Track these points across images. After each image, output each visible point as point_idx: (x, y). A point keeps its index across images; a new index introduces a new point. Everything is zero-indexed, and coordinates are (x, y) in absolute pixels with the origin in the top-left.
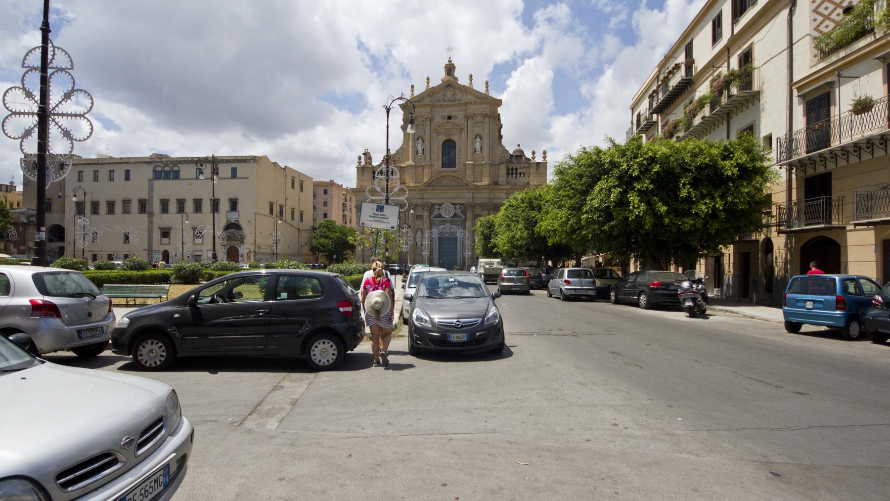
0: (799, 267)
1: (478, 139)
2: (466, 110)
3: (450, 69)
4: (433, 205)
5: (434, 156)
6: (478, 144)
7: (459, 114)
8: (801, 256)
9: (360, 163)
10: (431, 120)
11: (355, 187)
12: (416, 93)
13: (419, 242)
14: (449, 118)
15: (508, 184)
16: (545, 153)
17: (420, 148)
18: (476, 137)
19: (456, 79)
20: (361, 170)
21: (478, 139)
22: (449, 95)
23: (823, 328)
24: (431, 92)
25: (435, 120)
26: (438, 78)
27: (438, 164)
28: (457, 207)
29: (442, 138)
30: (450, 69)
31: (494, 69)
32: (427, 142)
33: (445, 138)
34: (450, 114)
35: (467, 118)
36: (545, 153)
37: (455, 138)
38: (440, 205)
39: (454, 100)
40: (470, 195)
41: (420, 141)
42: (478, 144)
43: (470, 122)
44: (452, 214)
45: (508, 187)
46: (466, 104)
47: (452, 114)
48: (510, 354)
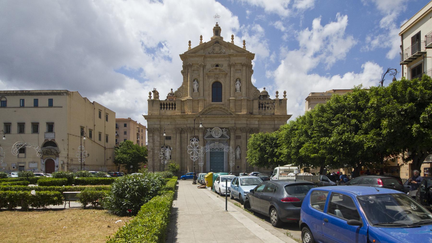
1: (238, 82)
3: (217, 30)
6: (238, 85)
12: (192, 47)
14: (217, 66)
16: (285, 93)
17: (195, 87)
18: (237, 80)
21: (238, 82)
22: (217, 49)
28: (224, 130)
30: (217, 30)
32: (201, 83)
33: (214, 81)
34: (217, 63)
36: (285, 93)
37: (221, 81)
39: (220, 53)
42: (238, 85)
45: (260, 116)
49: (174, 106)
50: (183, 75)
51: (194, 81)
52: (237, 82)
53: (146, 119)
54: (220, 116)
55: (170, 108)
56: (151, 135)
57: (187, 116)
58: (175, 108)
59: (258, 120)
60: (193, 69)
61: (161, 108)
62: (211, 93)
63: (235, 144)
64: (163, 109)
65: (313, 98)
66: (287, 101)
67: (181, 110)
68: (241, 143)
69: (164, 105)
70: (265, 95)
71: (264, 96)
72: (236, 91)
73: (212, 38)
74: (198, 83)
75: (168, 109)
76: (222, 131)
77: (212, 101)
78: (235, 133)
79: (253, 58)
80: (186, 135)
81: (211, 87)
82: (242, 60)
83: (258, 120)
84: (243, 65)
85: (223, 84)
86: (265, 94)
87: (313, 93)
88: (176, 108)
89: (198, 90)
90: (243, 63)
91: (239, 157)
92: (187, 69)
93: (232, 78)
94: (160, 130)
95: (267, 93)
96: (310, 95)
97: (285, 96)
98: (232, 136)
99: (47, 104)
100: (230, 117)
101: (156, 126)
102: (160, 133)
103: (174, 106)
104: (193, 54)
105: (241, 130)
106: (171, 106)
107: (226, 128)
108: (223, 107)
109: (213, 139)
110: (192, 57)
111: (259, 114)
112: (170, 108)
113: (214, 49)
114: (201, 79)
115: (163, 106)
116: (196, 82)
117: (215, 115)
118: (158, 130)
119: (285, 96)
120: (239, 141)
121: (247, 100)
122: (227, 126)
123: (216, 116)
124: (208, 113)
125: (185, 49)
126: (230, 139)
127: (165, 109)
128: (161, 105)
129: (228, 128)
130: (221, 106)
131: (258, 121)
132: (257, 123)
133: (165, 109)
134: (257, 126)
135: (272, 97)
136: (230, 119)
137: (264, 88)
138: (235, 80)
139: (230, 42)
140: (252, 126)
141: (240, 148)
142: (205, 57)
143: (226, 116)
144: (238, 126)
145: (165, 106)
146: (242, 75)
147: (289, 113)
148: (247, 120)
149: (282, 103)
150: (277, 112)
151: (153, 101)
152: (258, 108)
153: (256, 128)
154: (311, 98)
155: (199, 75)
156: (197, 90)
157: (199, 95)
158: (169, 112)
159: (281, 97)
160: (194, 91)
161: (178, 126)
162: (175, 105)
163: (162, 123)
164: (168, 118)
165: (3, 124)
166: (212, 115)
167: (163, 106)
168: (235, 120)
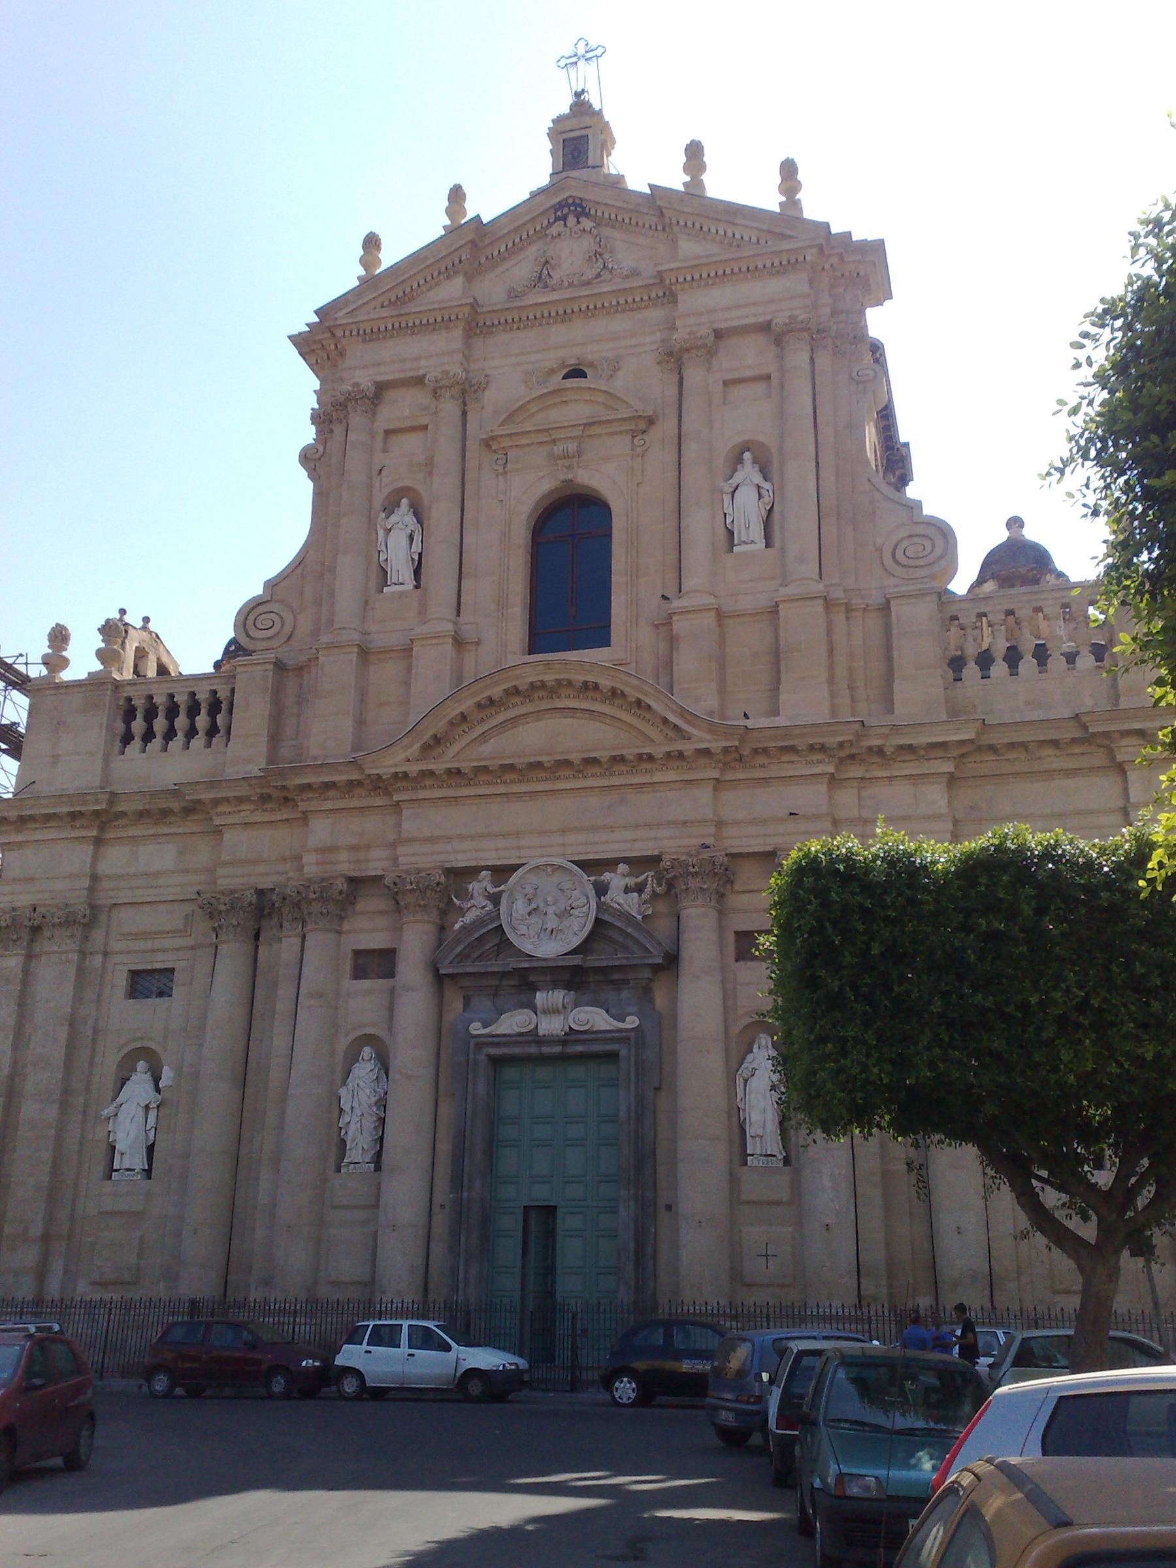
4: (461, 875)
5: (481, 591)
7: (626, 349)
8: (408, 1489)
10: (467, 392)
11: (833, 231)
12: (389, 256)
22: (571, 253)
24: (470, 245)
26: (511, 175)
27: (502, 629)
28: (617, 880)
29: (528, 487)
31: (313, 474)
32: (442, 514)
35: (674, 359)
37: (602, 475)
38: (502, 872)
43: (694, 375)
44: (576, 932)
46: (664, 291)
47: (591, 353)
51: (390, 508)
74: (420, 522)
76: (601, 889)
81: (521, 535)
83: (948, 767)
85: (617, 507)
89: (417, 572)
107: (638, 864)
128: (129, 714)
131: (952, 780)
148: (833, 781)
155: (429, 467)
167: (138, 725)
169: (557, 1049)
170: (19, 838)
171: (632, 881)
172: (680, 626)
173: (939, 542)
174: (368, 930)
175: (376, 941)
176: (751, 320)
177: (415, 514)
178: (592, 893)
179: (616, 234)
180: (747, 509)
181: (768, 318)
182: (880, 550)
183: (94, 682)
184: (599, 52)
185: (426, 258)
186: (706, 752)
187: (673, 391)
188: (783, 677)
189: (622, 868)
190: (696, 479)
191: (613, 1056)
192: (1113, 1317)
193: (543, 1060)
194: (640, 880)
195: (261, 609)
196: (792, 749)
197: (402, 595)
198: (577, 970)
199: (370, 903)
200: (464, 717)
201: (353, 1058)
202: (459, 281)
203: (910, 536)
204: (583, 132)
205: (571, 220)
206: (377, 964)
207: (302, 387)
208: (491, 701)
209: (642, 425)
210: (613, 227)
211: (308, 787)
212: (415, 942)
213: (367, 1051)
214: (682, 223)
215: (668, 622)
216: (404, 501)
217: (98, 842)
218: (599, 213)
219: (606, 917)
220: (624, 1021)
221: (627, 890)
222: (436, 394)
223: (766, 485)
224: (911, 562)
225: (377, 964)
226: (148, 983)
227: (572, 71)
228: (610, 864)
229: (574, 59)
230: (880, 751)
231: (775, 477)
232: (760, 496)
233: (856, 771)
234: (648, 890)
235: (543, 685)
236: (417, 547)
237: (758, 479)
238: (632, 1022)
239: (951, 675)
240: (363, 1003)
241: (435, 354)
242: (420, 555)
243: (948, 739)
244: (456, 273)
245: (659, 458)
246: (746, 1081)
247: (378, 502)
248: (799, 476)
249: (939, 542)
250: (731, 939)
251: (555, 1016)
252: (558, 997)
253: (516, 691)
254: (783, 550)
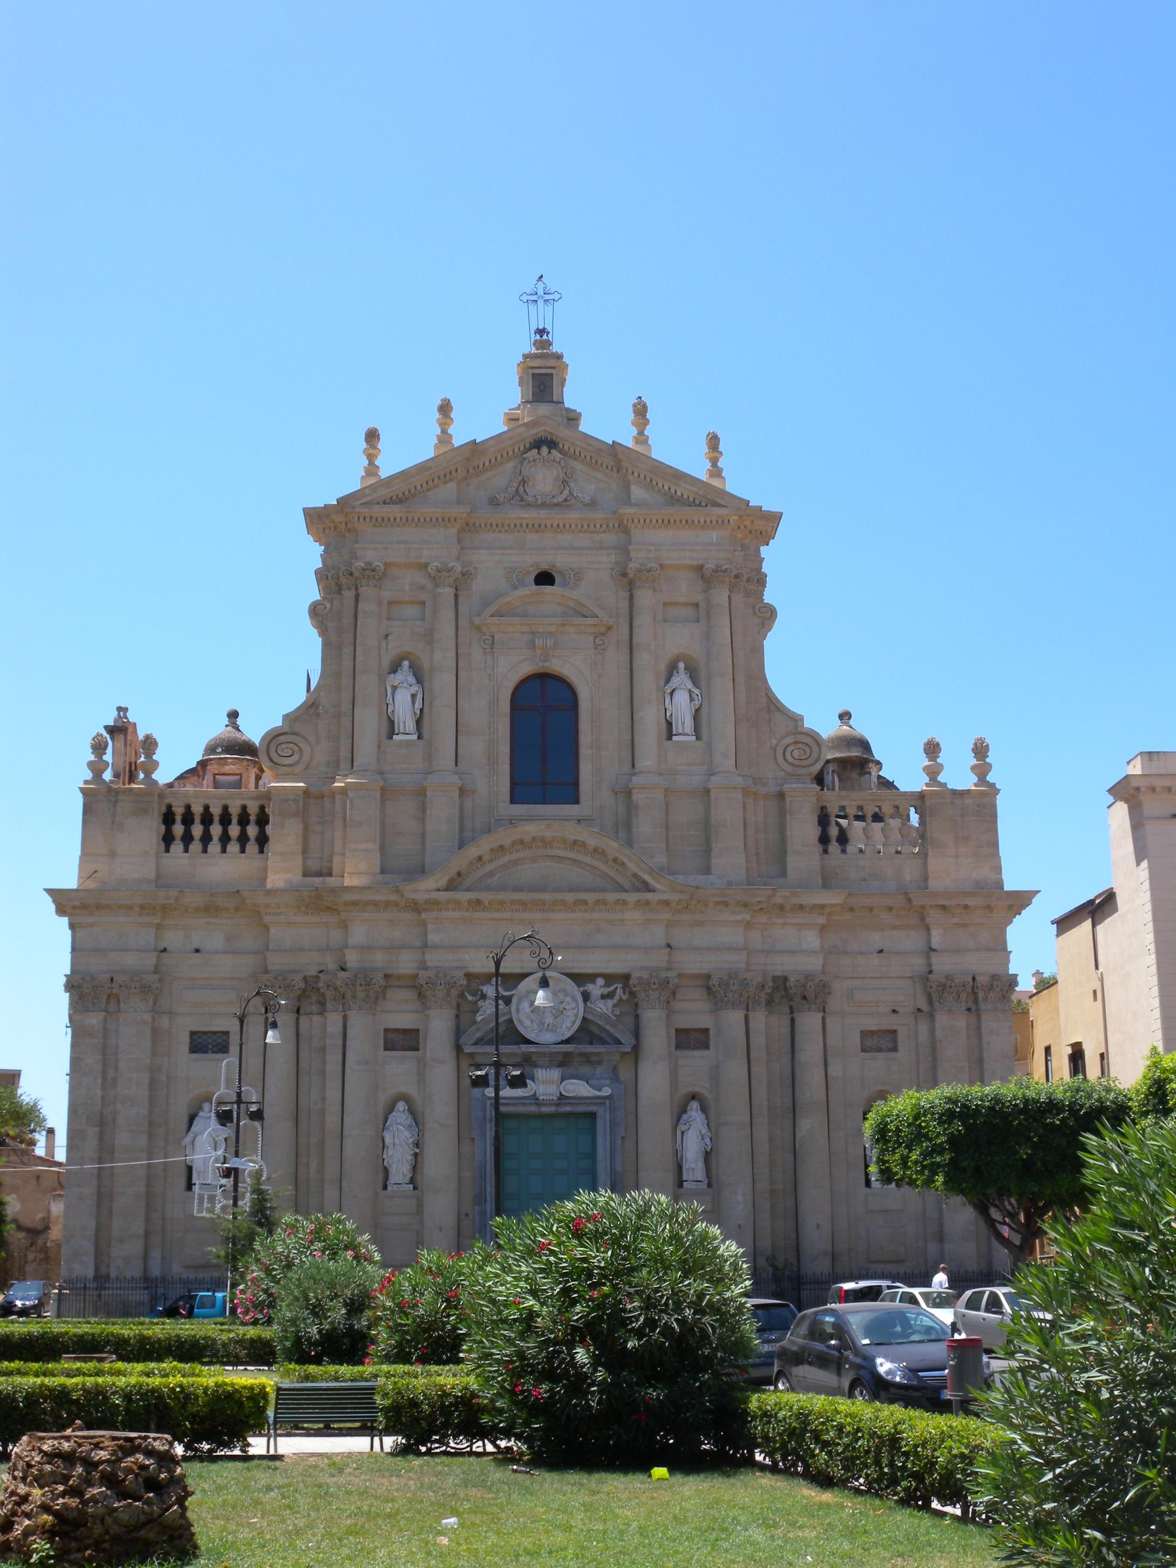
0: (573, 1477)
1: (681, 679)
2: (624, 550)
3: (543, 378)
5: (475, 747)
6: (681, 698)
9: (97, 768)
10: (461, 583)
11: (75, 887)
12: (388, 467)
13: (400, 1171)
14: (545, 578)
15: (827, 882)
16: (981, 750)
17: (403, 708)
18: (672, 670)
19: (573, 418)
20: (101, 803)
21: (681, 679)
22: (544, 478)
23: (358, 1425)
25: (478, 585)
26: (489, 408)
28: (596, 989)
29: (513, 667)
30: (543, 378)
32: (444, 682)
33: (527, 669)
34: (544, 562)
36: (981, 750)
37: (572, 666)
39: (565, 505)
40: (658, 934)
41: (404, 676)
42: (681, 698)
43: (645, 598)
45: (832, 898)
48: (304, 509)
49: (252, 831)
50: (323, 632)
51: (394, 668)
52: (676, 681)
53: (61, 911)
54: (570, 897)
55: (225, 839)
56: (94, 1020)
57: (348, 897)
58: (262, 840)
59: (821, 920)
60: (386, 595)
61: (168, 839)
62: (505, 748)
63: (674, 1084)
64: (177, 847)
65: (1159, 783)
66: (1000, 800)
67: (305, 851)
68: (715, 1074)
69: (188, 819)
70: (856, 760)
71: (844, 764)
72: (670, 735)
73: (511, 419)
74: (419, 681)
75: (215, 847)
76: (586, 997)
77: (513, 801)
78: (670, 1013)
79: (766, 537)
80: (333, 1020)
81: (505, 707)
82: (707, 544)
83: (821, 920)
84: (706, 577)
85: (583, 693)
86: (855, 753)
87: (1149, 756)
88: (271, 846)
89: (419, 722)
90: (710, 566)
91: (700, 1174)
92: (345, 599)
93: (643, 658)
94: (152, 986)
95: (865, 745)
96: (1136, 769)
97: (982, 770)
98: (656, 1037)
99: (257, 1124)
100: (638, 904)
101: (130, 960)
102: (156, 1012)
103: (252, 831)
104: (395, 511)
105: (713, 989)
106: (234, 830)
107: (609, 979)
108: (592, 842)
109: (525, 1048)
110: (380, 522)
111: (826, 885)
112: (225, 839)
113: (524, 482)
114: (443, 656)
115: (178, 829)
116: (404, 676)
117: (532, 889)
118: (145, 989)
119: (982, 770)
120: (696, 1064)
121: (746, 792)
122: (615, 964)
123: (547, 897)
124: (491, 874)
125: (341, 479)
126: (636, 1050)
127: (196, 846)
128: (168, 818)
129: (625, 978)
130: (573, 832)
131: (823, 929)
132: (812, 939)
133: (196, 846)
134: (813, 964)
135: (904, 771)
136: (636, 915)
137: (845, 716)
138: (663, 667)
139: (629, 443)
140: (781, 965)
141: (704, 1109)
142: (469, 527)
143: (611, 897)
144: (693, 964)
145: (197, 830)
146: (708, 636)
147: (1012, 882)
148: (748, 925)
149: (970, 815)
150: (948, 870)
151: (111, 793)
152: (819, 848)
153: (809, 976)
154: (1142, 784)
155: (429, 637)
156: (411, 725)
157: (429, 757)
158: (223, 867)
159: (958, 775)
160: (391, 731)
161: (276, 962)
162: (263, 820)
163: (173, 939)
164: (210, 910)
165: (769, 506)
166: (517, 889)
167: (178, 829)
168: (669, 924)
169: (553, 1109)
170: (91, 920)
171: (606, 991)
172: (637, 797)
173: (815, 748)
174: (400, 1013)
175: (403, 1020)
176: (688, 562)
177: (415, 675)
178: (580, 999)
179: (579, 466)
180: (682, 706)
181: (700, 562)
182: (774, 749)
183: (1022, 1239)
184: (556, 296)
185: (430, 468)
186: (666, 903)
187: (624, 604)
188: (714, 845)
189: (600, 981)
190: (647, 681)
191: (592, 1116)
192: (889, 1283)
193: (541, 1116)
194: (611, 989)
195: (282, 739)
196: (726, 904)
197: (409, 744)
198: (567, 1055)
199: (401, 997)
200: (480, 858)
201: (391, 1109)
202: (452, 486)
203: (795, 743)
204: (549, 371)
205: (545, 450)
206: (404, 1041)
207: (312, 554)
208: (502, 847)
209: (603, 629)
210: (576, 459)
211: (354, 904)
212: (438, 1027)
213: (401, 1106)
214: (636, 474)
215: (629, 793)
216: (406, 663)
217: (159, 927)
218: (566, 448)
219: (590, 1017)
220: (600, 1090)
221: (603, 997)
222: (435, 580)
223: (697, 691)
224: (796, 762)
225: (404, 1041)
226: (206, 1043)
227: (532, 307)
228: (592, 978)
229: (534, 298)
230: (782, 908)
231: (703, 684)
232: (692, 700)
233: (763, 919)
234: (617, 997)
235: (543, 840)
236: (418, 705)
237: (690, 685)
238: (606, 1092)
239: (820, 848)
240: (399, 1071)
241: (438, 547)
242: (421, 710)
243: (827, 902)
244: (451, 480)
245: (615, 658)
246: (683, 1133)
247: (386, 663)
248: (722, 689)
249: (815, 748)
250: (673, 1033)
251: (546, 1084)
252: (555, 1074)
253: (521, 842)
254: (709, 744)
